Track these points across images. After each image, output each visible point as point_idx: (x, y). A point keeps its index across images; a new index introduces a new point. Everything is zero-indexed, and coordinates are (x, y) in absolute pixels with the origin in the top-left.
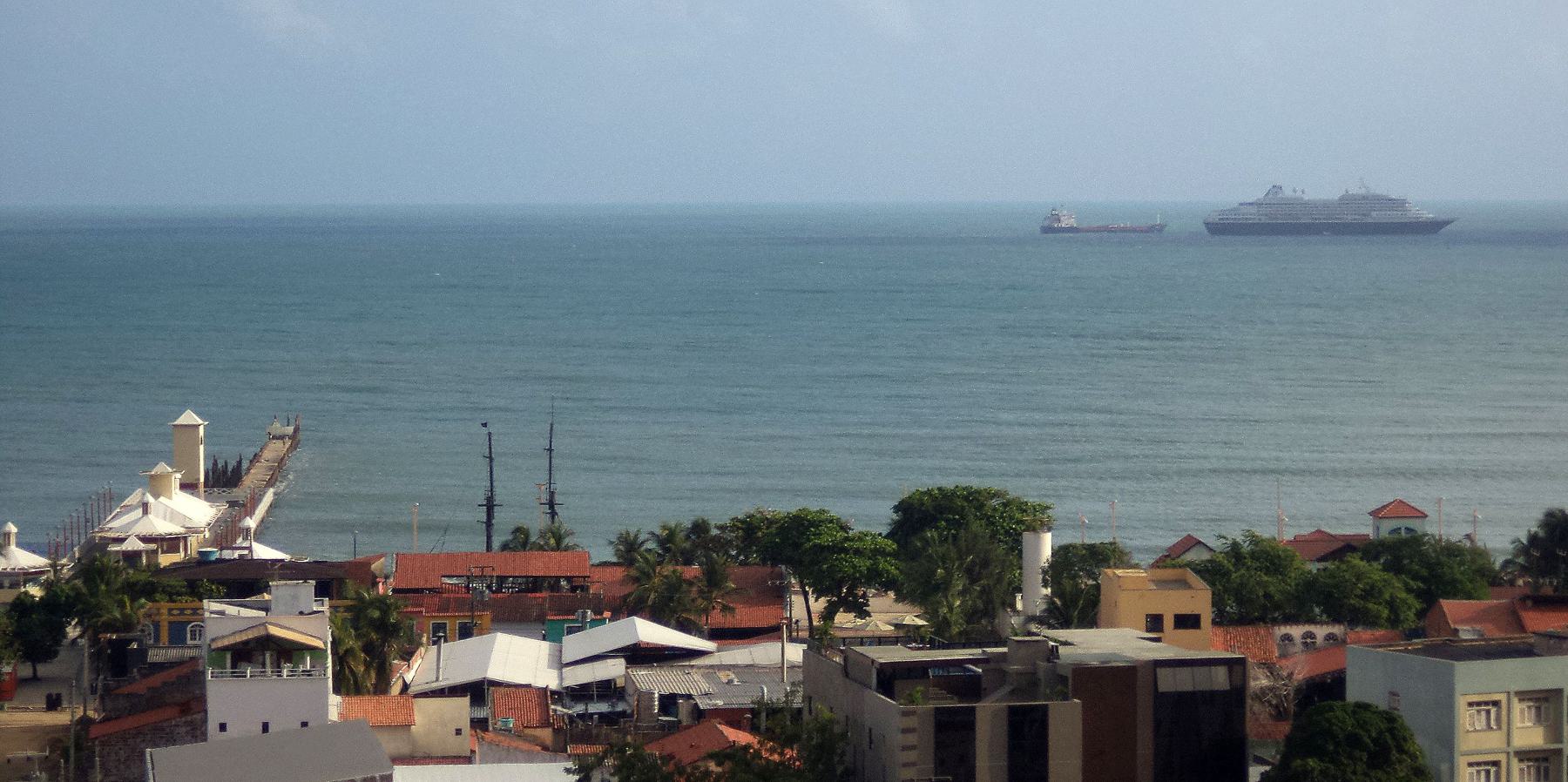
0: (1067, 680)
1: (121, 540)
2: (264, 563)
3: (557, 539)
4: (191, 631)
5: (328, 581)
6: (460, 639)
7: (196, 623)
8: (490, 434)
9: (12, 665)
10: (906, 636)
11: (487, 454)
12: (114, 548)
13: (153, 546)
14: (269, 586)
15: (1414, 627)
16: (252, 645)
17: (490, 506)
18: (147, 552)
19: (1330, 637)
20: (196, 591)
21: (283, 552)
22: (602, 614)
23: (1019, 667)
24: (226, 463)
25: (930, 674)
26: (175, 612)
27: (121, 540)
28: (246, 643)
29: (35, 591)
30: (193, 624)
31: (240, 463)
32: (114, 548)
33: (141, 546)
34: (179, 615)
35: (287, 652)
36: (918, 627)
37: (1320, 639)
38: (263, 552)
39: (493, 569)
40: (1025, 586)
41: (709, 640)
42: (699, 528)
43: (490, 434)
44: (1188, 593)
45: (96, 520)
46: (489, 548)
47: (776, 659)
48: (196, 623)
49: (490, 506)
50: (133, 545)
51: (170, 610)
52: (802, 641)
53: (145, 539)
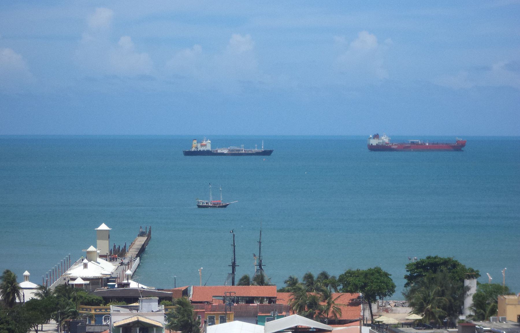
0: (281, 314)
2: (135, 290)
4: (104, 319)
5: (162, 299)
6: (220, 323)
7: (107, 315)
8: (234, 235)
11: (233, 244)
14: (139, 300)
15: (196, 150)
16: (131, 325)
17: (234, 266)
18: (85, 284)
20: (107, 300)
21: (400, 330)
22: (282, 313)
25: (228, 312)
26: (89, 310)
28: (128, 324)
29: (190, 321)
30: (105, 315)
33: (83, 282)
36: (420, 320)
38: (133, 285)
39: (235, 293)
40: (498, 308)
41: (328, 325)
43: (234, 235)
45: (63, 270)
48: (107, 315)
49: (234, 266)
50: (79, 281)
52: (368, 325)
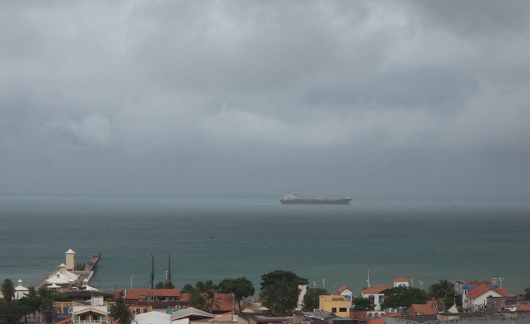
1: (51, 285)
2: (89, 292)
3: (170, 286)
5: (107, 297)
8: (153, 257)
9: (152, 301)
10: (264, 313)
12: (49, 287)
13: (60, 287)
19: (382, 314)
23: (96, 290)
24: (81, 264)
26: (60, 304)
27: (51, 285)
31: (84, 264)
32: (49, 287)
34: (58, 305)
35: (96, 316)
37: (379, 315)
38: (89, 288)
42: (210, 282)
43: (153, 257)
44: (343, 302)
46: (152, 288)
47: (230, 319)
50: (54, 286)
51: (64, 304)
53: (57, 285)
